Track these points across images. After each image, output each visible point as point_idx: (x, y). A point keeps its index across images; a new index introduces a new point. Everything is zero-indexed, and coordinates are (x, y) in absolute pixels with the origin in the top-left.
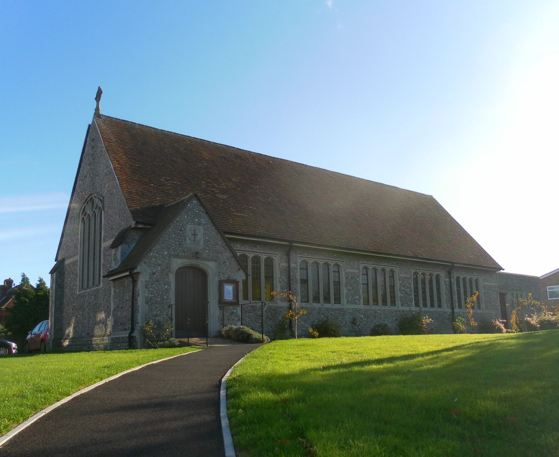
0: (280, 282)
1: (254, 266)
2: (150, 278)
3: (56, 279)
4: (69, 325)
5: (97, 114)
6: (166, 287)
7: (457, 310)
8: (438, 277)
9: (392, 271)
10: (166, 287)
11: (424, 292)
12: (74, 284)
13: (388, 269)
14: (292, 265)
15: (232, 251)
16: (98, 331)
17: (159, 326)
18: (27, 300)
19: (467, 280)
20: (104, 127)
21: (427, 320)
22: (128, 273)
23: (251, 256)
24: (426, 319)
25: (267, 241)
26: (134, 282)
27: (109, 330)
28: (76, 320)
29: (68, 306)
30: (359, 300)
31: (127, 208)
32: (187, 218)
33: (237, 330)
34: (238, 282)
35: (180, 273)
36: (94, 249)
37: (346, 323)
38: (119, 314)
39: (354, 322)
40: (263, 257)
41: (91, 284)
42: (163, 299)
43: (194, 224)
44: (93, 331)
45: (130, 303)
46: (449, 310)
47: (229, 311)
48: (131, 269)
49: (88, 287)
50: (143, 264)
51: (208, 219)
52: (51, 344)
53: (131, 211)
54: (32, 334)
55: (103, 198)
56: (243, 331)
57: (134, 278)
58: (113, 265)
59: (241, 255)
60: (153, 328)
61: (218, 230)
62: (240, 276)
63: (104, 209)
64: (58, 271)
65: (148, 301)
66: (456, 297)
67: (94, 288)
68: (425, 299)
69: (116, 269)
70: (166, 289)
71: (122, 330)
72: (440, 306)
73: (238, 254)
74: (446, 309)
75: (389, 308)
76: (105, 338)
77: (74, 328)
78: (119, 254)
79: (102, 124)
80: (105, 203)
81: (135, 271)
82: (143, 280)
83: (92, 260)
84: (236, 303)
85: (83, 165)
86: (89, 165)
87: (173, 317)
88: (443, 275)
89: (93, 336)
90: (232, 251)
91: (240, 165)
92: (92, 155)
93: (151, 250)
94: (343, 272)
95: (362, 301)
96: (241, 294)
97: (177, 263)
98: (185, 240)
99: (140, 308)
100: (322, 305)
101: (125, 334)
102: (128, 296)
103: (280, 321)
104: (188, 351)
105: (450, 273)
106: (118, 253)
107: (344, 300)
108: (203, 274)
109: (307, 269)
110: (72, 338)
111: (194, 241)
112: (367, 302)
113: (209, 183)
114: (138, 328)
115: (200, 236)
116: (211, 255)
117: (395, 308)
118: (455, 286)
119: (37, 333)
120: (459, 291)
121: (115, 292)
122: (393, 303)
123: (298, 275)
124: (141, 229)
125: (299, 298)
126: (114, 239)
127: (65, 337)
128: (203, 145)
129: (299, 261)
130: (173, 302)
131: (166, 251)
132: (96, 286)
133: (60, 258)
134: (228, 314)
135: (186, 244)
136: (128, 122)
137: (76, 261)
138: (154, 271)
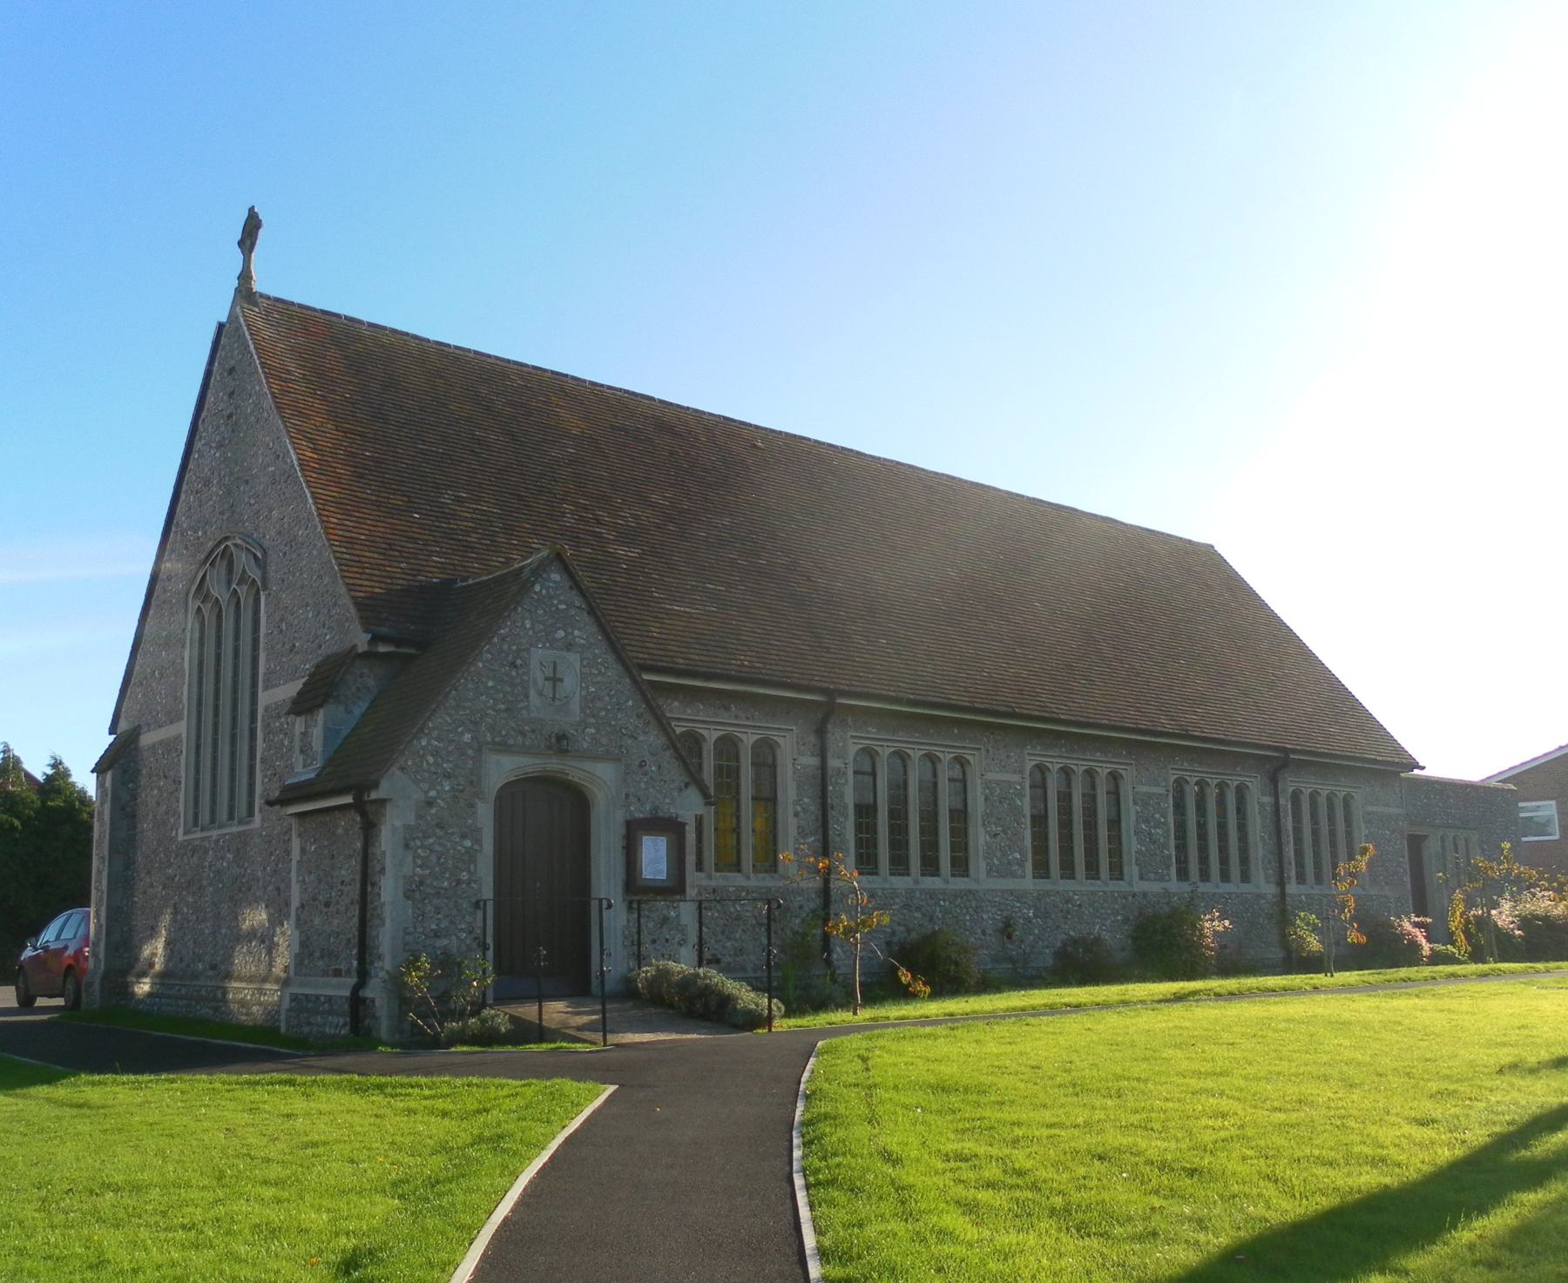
0: (796, 814)
1: (721, 767)
2: (419, 817)
3: (114, 791)
4: (153, 932)
5: (245, 291)
6: (468, 843)
7: (1292, 888)
8: (1241, 792)
9: (1114, 777)
10: (468, 843)
11: (1202, 837)
12: (168, 803)
13: (1103, 771)
14: (833, 763)
15: (663, 723)
16: (244, 961)
17: (448, 965)
18: (17, 823)
19: (1322, 800)
20: (266, 334)
21: (1213, 925)
22: (348, 799)
23: (711, 735)
24: (1212, 920)
25: (762, 691)
26: (369, 829)
27: (283, 960)
28: (174, 920)
29: (148, 873)
30: (1021, 864)
31: (343, 590)
32: (532, 627)
33: (687, 983)
34: (683, 825)
35: (512, 796)
36: (234, 708)
37: (984, 933)
38: (317, 921)
39: (1006, 930)
40: (748, 739)
41: (223, 813)
42: (459, 882)
43: (552, 647)
44: (228, 959)
45: (354, 892)
46: (1270, 890)
47: (654, 915)
48: (360, 790)
49: (213, 821)
50: (399, 773)
51: (594, 629)
52: (97, 986)
53: (358, 604)
54: (36, 949)
55: (265, 552)
56: (707, 986)
57: (368, 817)
58: (299, 768)
59: (683, 734)
60: (428, 977)
61: (624, 664)
62: (689, 807)
63: (265, 587)
64: (119, 761)
65: (413, 890)
66: (1290, 851)
67: (235, 829)
68: (1204, 859)
69: (309, 782)
70: (468, 851)
71: (325, 974)
72: (1245, 877)
73: (678, 731)
74: (1263, 885)
75: (1105, 885)
76: (268, 986)
77: (168, 943)
78: (317, 733)
79: (260, 324)
80: (272, 568)
81: (374, 795)
82: (398, 823)
83: (227, 739)
84: (674, 888)
85: (198, 445)
86: (220, 446)
87: (490, 941)
88: (1255, 785)
89: (228, 976)
90: (663, 723)
91: (671, 453)
92: (230, 416)
93: (421, 729)
94: (979, 782)
95: (1029, 865)
96: (691, 859)
97: (502, 769)
98: (527, 696)
99: (387, 913)
100: (917, 882)
101: (341, 988)
102: (348, 870)
103: (795, 933)
104: (578, 1106)
105: (1274, 780)
106: (316, 729)
107: (978, 865)
108: (577, 801)
109: (874, 774)
110: (164, 975)
111: (554, 699)
112: (1041, 869)
113: (585, 508)
114: (382, 974)
115: (570, 683)
116: (604, 741)
117: (1122, 886)
118: (1290, 818)
119: (52, 946)
120: (1298, 830)
121: (303, 851)
122: (1117, 871)
123: (847, 794)
124: (388, 655)
125: (851, 860)
126: (298, 685)
127: (138, 968)
128: (562, 389)
129: (853, 749)
130: (488, 892)
131: (469, 731)
132: (240, 823)
133: (123, 726)
134: (651, 925)
135: (527, 708)
136: (338, 316)
137: (178, 738)
138: (433, 793)
